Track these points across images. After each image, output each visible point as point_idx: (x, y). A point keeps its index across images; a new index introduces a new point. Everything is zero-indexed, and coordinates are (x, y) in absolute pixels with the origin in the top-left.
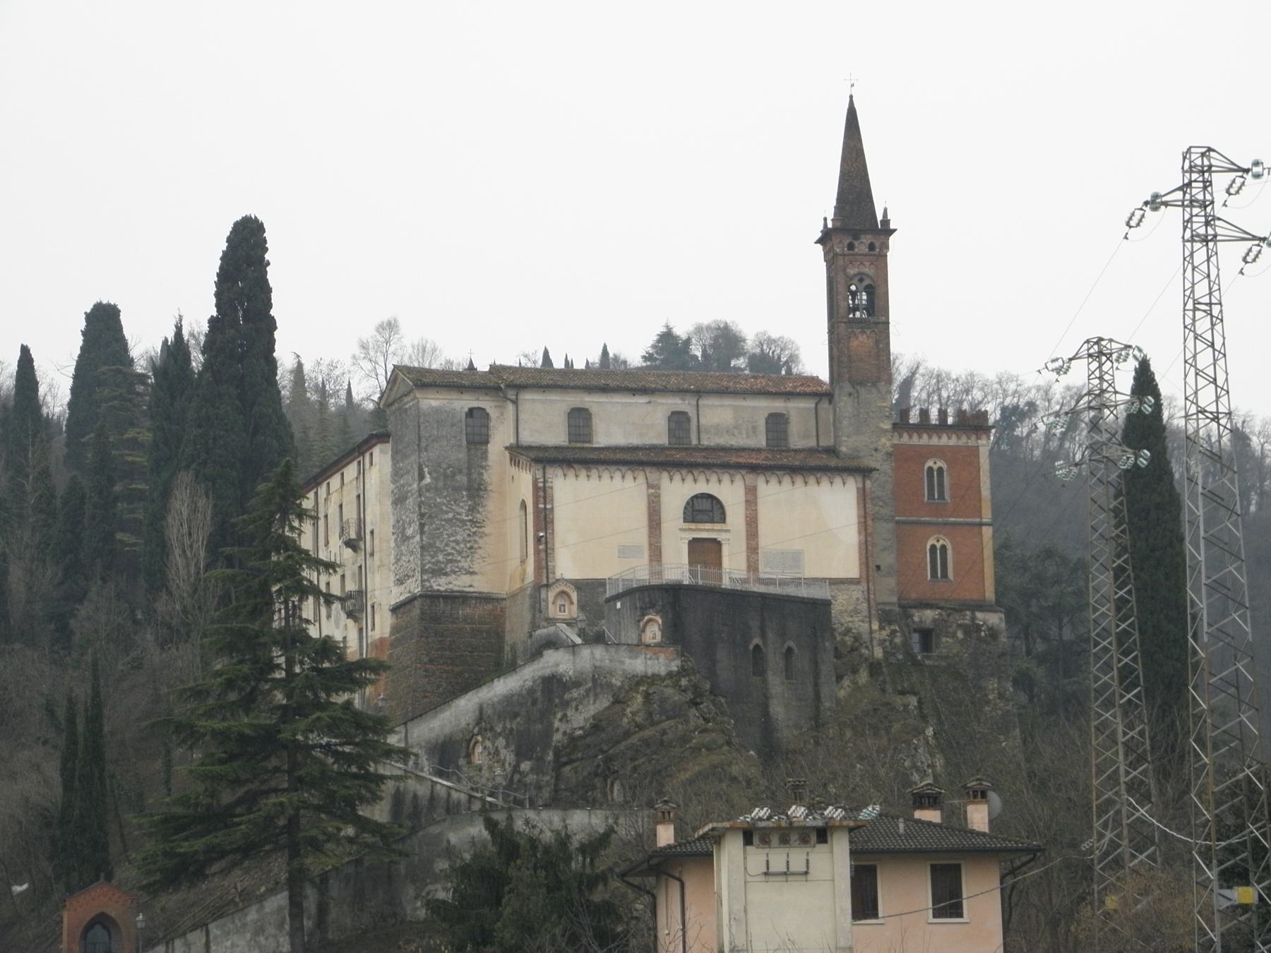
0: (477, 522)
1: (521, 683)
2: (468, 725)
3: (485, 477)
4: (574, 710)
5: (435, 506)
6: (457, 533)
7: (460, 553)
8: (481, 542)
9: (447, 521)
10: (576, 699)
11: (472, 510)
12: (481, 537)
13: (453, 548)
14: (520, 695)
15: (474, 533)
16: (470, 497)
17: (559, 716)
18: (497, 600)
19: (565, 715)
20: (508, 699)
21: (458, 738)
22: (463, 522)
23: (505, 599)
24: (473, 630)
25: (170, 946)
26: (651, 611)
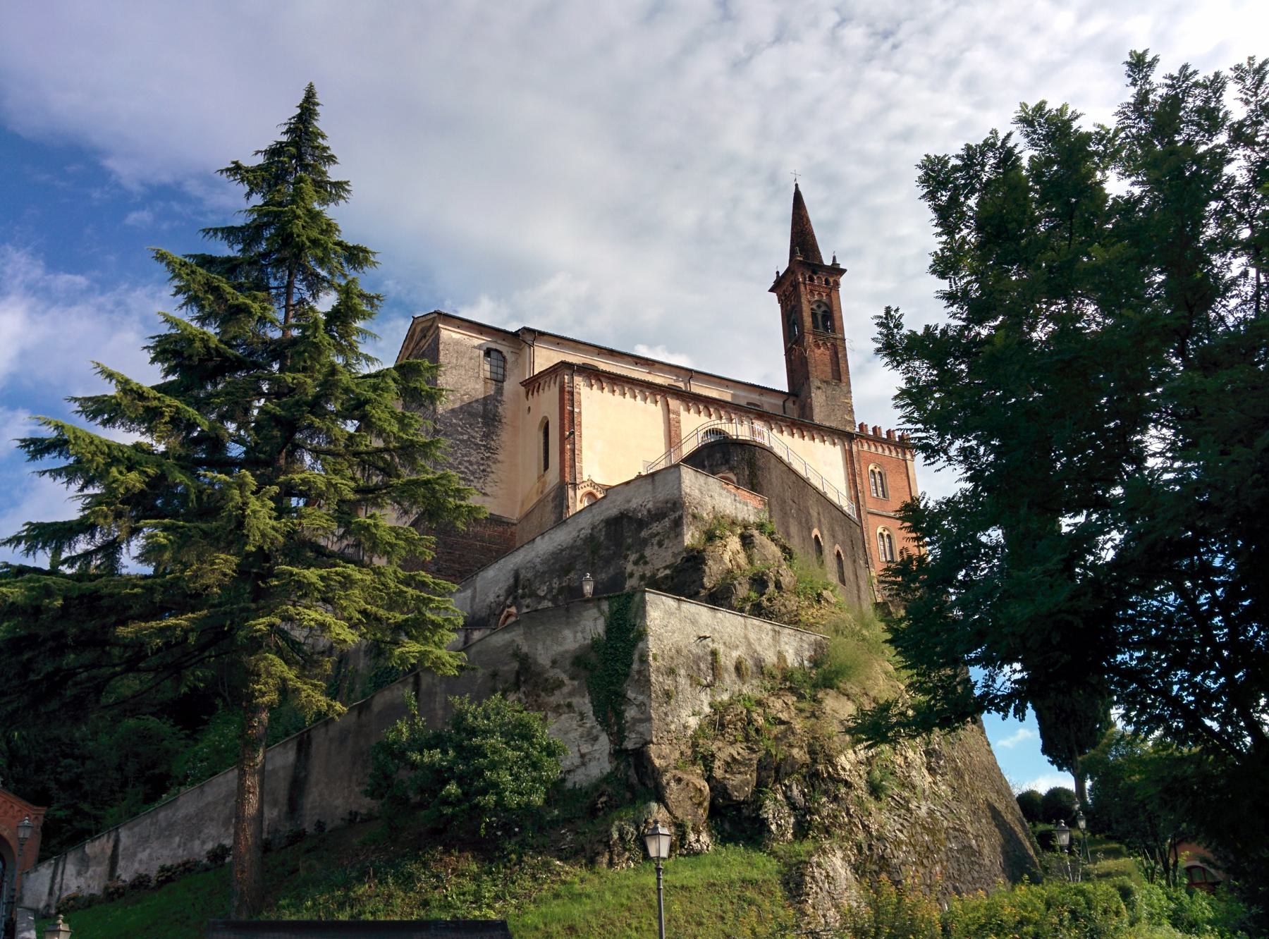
0: (490, 448)
1: (575, 534)
2: (498, 597)
3: (500, 410)
4: (656, 547)
5: (451, 425)
6: (471, 455)
7: (473, 473)
8: (494, 467)
9: (462, 441)
10: (658, 534)
11: (486, 436)
12: (494, 463)
13: (466, 468)
14: (572, 547)
15: (488, 458)
16: (485, 424)
17: (633, 557)
18: (508, 523)
19: (642, 557)
20: (556, 555)
21: (483, 614)
22: (476, 444)
23: (515, 525)
24: (482, 547)
25: (61, 865)
26: (723, 468)
